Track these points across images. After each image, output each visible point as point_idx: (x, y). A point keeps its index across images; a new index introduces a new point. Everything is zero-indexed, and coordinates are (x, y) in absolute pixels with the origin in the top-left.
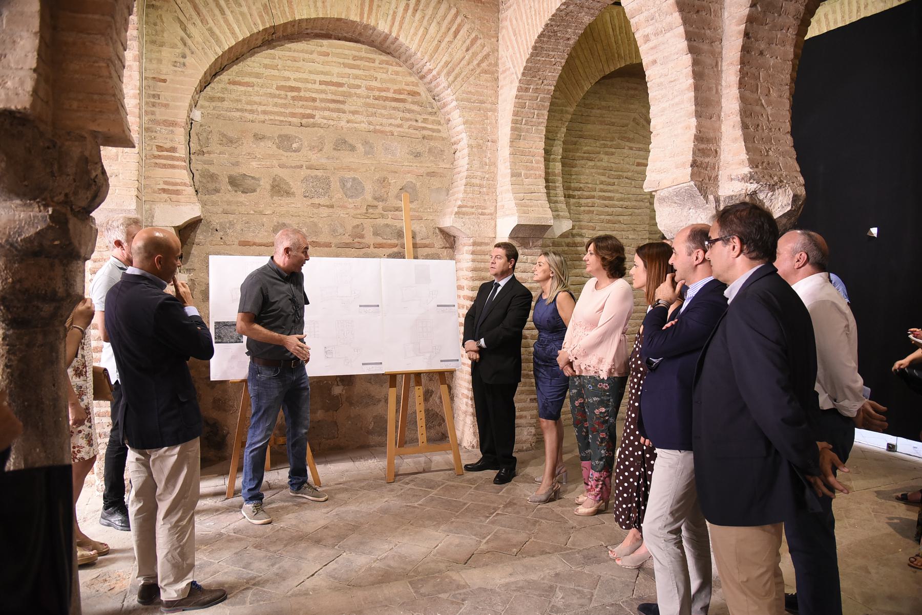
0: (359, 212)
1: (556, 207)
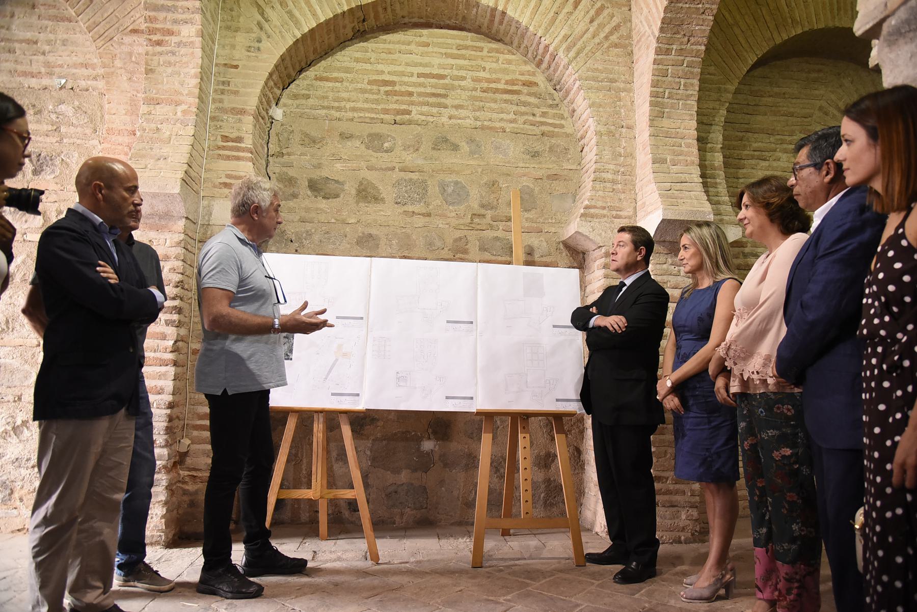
0: (462, 221)
1: (718, 209)
